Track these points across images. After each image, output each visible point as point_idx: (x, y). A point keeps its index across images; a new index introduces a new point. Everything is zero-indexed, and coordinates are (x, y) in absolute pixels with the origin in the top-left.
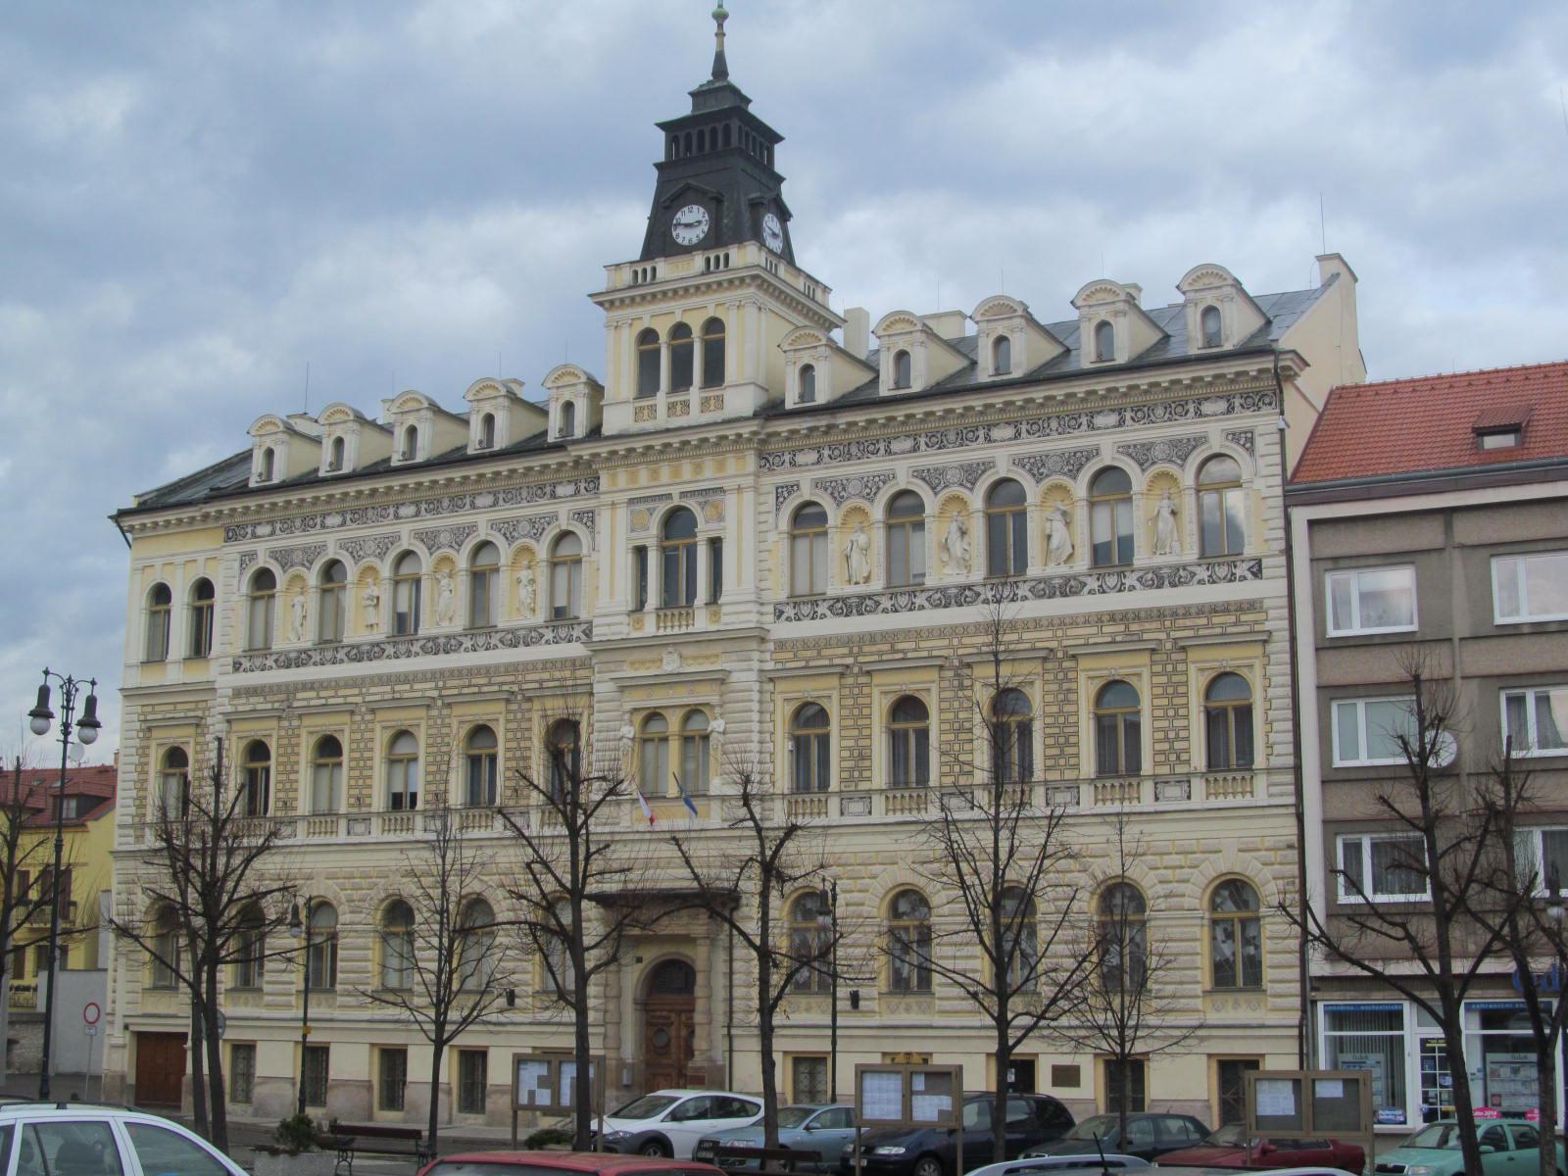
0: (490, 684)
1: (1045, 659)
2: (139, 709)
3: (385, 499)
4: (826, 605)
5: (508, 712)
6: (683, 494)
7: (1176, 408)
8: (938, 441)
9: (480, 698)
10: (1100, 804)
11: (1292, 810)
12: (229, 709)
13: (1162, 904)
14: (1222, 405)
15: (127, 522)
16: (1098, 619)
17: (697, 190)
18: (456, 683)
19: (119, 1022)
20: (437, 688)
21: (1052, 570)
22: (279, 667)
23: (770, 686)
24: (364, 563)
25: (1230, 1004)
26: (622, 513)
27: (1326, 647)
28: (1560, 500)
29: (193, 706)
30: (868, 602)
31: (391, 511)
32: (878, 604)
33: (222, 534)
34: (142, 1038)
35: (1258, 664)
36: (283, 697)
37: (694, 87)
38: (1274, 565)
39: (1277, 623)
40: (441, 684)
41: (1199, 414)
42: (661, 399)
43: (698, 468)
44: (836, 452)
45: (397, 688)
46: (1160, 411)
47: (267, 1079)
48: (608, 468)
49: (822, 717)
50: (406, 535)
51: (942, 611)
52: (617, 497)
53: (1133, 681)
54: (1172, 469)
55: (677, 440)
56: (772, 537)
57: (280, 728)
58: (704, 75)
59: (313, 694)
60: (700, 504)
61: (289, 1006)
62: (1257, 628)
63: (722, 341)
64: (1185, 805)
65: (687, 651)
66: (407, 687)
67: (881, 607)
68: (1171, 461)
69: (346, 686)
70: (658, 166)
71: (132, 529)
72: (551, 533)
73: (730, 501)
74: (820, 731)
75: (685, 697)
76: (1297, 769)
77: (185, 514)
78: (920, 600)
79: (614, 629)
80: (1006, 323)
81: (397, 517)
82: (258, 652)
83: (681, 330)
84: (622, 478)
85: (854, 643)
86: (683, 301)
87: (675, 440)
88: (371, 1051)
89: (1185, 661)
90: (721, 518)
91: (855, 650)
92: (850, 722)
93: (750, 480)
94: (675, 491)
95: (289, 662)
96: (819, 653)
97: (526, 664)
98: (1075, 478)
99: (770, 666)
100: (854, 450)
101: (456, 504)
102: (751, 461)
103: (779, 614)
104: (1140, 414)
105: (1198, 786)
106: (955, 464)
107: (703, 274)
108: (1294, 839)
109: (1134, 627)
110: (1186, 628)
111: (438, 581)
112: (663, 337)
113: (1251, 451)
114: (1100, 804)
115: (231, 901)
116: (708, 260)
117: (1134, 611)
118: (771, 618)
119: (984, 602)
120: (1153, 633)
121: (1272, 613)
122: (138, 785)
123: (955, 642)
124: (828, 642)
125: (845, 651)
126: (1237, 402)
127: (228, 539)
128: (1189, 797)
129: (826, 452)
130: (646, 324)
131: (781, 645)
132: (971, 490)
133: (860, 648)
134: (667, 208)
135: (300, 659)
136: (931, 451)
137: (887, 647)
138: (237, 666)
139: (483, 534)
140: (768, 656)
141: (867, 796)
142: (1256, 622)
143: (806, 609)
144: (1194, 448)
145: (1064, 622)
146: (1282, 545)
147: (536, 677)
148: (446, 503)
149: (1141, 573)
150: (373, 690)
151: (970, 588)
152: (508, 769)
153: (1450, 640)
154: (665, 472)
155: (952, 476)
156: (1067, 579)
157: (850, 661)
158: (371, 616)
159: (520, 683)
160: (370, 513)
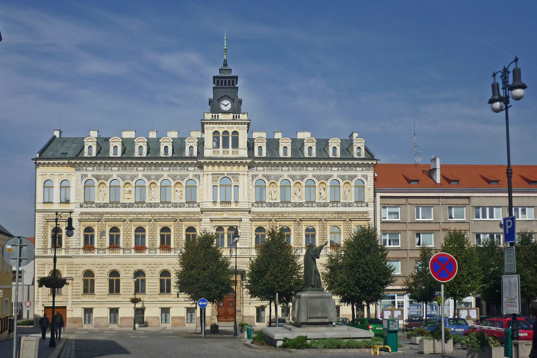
9: (166, 220)
12: (79, 218)
17: (228, 97)
18: (158, 215)
19: (40, 303)
21: (321, 201)
24: (271, 181)
26: (210, 177)
27: (382, 223)
34: (46, 308)
35: (198, 225)
39: (371, 216)
42: (221, 149)
49: (314, 230)
52: (209, 173)
54: (349, 181)
56: (251, 187)
59: (193, 215)
63: (238, 137)
69: (121, 214)
73: (241, 177)
78: (339, 205)
81: (111, 170)
82: (88, 203)
85: (273, 214)
87: (234, 161)
90: (238, 181)
94: (226, 173)
109: (340, 215)
113: (367, 180)
116: (234, 116)
118: (251, 206)
120: (344, 216)
131: (254, 213)
135: (105, 206)
138: (81, 206)
143: (260, 205)
145: (324, 213)
147: (184, 215)
151: (301, 203)
154: (222, 168)
156: (325, 203)
157: (272, 218)
159: (178, 217)
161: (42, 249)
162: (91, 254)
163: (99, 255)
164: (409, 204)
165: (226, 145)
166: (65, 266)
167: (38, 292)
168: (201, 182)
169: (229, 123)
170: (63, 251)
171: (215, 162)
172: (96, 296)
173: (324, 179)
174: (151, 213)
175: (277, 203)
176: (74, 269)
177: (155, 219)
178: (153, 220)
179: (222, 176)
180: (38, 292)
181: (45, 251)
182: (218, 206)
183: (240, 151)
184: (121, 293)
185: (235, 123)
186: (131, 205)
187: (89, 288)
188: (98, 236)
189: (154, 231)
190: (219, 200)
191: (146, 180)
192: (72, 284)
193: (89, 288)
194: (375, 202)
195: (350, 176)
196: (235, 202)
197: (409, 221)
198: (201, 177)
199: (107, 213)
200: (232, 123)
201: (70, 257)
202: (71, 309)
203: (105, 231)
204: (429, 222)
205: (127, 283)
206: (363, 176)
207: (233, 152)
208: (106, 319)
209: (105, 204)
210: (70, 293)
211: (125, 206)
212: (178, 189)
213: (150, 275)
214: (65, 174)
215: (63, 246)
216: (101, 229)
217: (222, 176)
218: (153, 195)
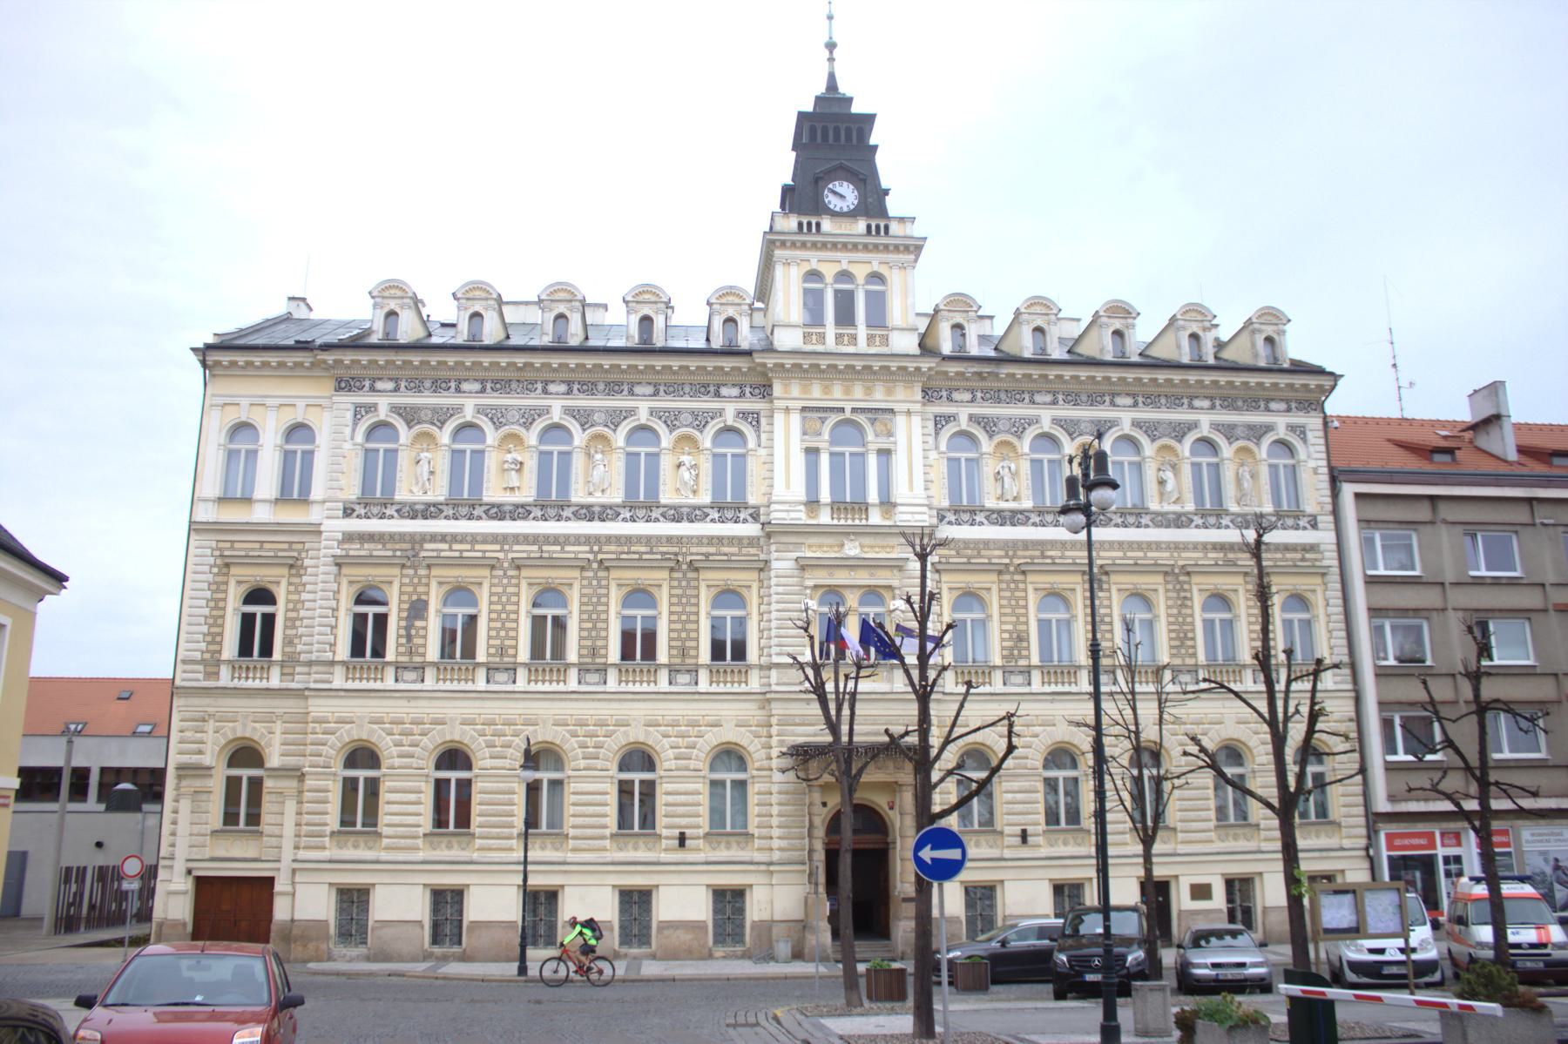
0: (651, 553)
2: (214, 544)
5: (583, 578)
6: (854, 410)
8: (589, 388)
9: (640, 564)
12: (339, 552)
13: (397, 762)
14: (477, 386)
15: (212, 357)
16: (1204, 547)
18: (613, 548)
19: (180, 866)
20: (591, 551)
21: (1167, 508)
22: (402, 517)
25: (723, 845)
26: (796, 419)
27: (1371, 581)
29: (286, 546)
32: (1028, 518)
33: (331, 384)
34: (201, 883)
35: (755, 586)
36: (405, 546)
38: (1326, 520)
39: (1330, 559)
40: (596, 548)
41: (545, 391)
43: (869, 391)
45: (545, 548)
47: (476, 925)
52: (791, 404)
54: (1251, 445)
56: (347, 446)
57: (402, 576)
58: (821, 89)
59: (445, 546)
61: (511, 849)
64: (510, 687)
65: (867, 541)
66: (558, 548)
69: (485, 542)
71: (218, 363)
73: (901, 421)
74: (739, 613)
75: (863, 578)
79: (793, 515)
81: (545, 391)
82: (373, 500)
84: (795, 390)
90: (890, 434)
92: (1008, 611)
94: (848, 406)
95: (413, 511)
97: (690, 538)
98: (528, 429)
100: (1003, 396)
101: (528, 386)
103: (941, 518)
105: (612, 675)
108: (1353, 715)
109: (1231, 556)
113: (1304, 440)
115: (947, 741)
121: (1327, 554)
122: (211, 621)
123: (596, 548)
124: (987, 544)
127: (339, 389)
129: (979, 395)
135: (429, 511)
137: (1037, 553)
138: (348, 512)
141: (1027, 671)
145: (1178, 547)
146: (1329, 508)
147: (704, 550)
148: (601, 387)
150: (516, 548)
152: (1003, 631)
153: (1543, 585)
154: (837, 391)
156: (1179, 515)
158: (514, 479)
159: (685, 554)
160: (514, 385)
161: (203, 662)
162: (372, 685)
163: (401, 686)
164: (1445, 522)
166: (278, 727)
167: (173, 834)
168: (764, 436)
169: (855, 247)
170: (275, 672)
171: (809, 367)
172: (385, 841)
173: (1169, 436)
174: (588, 540)
175: (1021, 512)
176: (310, 749)
177: (600, 562)
178: (595, 565)
179: (834, 418)
180: (174, 823)
181: (210, 669)
182: (825, 518)
184: (474, 828)
185: (876, 247)
186: (520, 512)
187: (360, 807)
188: (400, 619)
189: (599, 603)
190: (825, 496)
191: (574, 426)
192: (301, 792)
193: (360, 807)
194: (1336, 512)
195: (1251, 427)
196: (882, 503)
197: (1449, 577)
198: (763, 421)
199: (434, 538)
200: (866, 247)
201: (300, 694)
202: (289, 889)
203: (426, 603)
204: (1512, 583)
205: (497, 790)
206: (1292, 428)
208: (418, 930)
209: (428, 505)
210: (289, 829)
211: (498, 512)
212: (685, 458)
213: (582, 763)
214: (301, 403)
215: (277, 655)
216: (410, 594)
217: (834, 418)
218: (600, 477)
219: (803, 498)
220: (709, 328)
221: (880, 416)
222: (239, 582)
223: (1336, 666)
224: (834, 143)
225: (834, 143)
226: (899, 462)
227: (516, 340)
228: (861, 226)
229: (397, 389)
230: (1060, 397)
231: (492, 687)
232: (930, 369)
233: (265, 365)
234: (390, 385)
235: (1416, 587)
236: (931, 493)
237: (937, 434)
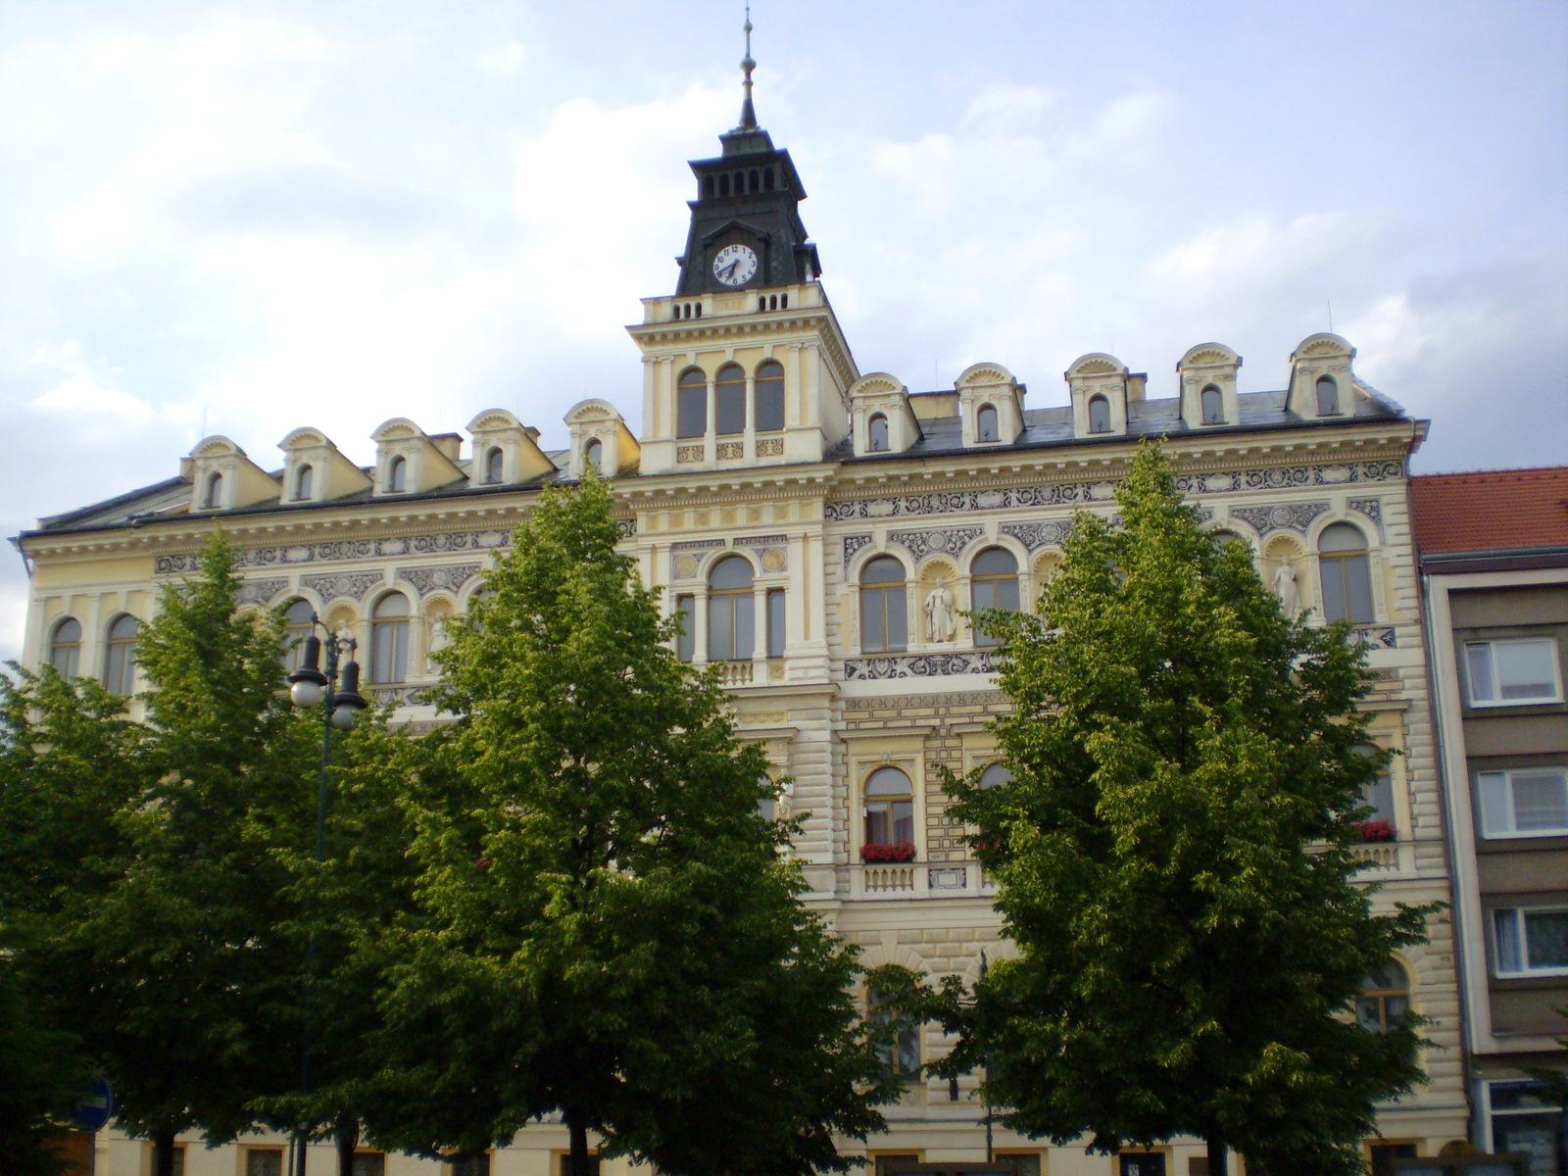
1: (927, 738)
3: (273, 541)
4: (906, 662)
6: (737, 541)
7: (1295, 474)
8: (428, 544)
10: (871, 890)
11: (1444, 883)
21: (933, 648)
23: (842, 748)
28: (1560, 587)
30: (955, 661)
31: (372, 546)
32: (966, 663)
33: (152, 565)
37: (725, 131)
41: (1319, 481)
43: (755, 514)
44: (915, 504)
46: (1277, 477)
48: (648, 510)
50: (389, 572)
51: (925, 679)
52: (658, 541)
53: (904, 766)
55: (976, 466)
58: (733, 122)
60: (757, 551)
62: (1394, 697)
67: (971, 666)
68: (1290, 527)
70: (692, 205)
72: (973, 548)
73: (794, 550)
76: (1446, 841)
77: (107, 540)
80: (1105, 382)
83: (730, 369)
84: (663, 522)
86: (735, 341)
88: (552, 1157)
89: (960, 748)
90: (783, 567)
91: (942, 711)
93: (818, 529)
96: (899, 713)
99: (842, 725)
100: (935, 502)
101: (359, 549)
102: (817, 510)
103: (850, 671)
104: (1255, 479)
106: (1052, 522)
107: (670, 322)
110: (961, 715)
111: (431, 626)
112: (711, 377)
113: (1376, 519)
114: (871, 890)
116: (762, 301)
117: (959, 694)
118: (841, 675)
119: (973, 670)
121: (1408, 683)
124: (909, 701)
125: (930, 711)
126: (1243, 479)
127: (160, 570)
128: (964, 885)
129: (903, 504)
130: (690, 361)
131: (854, 704)
132: (456, 593)
133: (948, 709)
134: (706, 247)
136: (1024, 507)
137: (979, 709)
139: (390, 582)
140: (839, 715)
142: (1392, 691)
143: (882, 667)
144: (1316, 514)
146: (1415, 614)
147: (968, 709)
148: (441, 540)
149: (912, 660)
154: (715, 518)
155: (1276, 517)
157: (936, 722)
160: (345, 548)
165: (730, 423)
173: (941, 550)
183: (789, 440)
194: (1423, 621)
207: (721, 450)
219: (765, 655)
220: (1289, 393)
221: (771, 546)
222: (861, 763)
223: (1416, 842)
224: (747, 196)
225: (747, 196)
226: (792, 603)
227: (1037, 436)
228: (751, 301)
229: (311, 558)
230: (1014, 496)
231: (937, 893)
232: (827, 479)
233: (84, 550)
234: (398, 546)
235: (1553, 721)
236: (833, 640)
237: (847, 561)
